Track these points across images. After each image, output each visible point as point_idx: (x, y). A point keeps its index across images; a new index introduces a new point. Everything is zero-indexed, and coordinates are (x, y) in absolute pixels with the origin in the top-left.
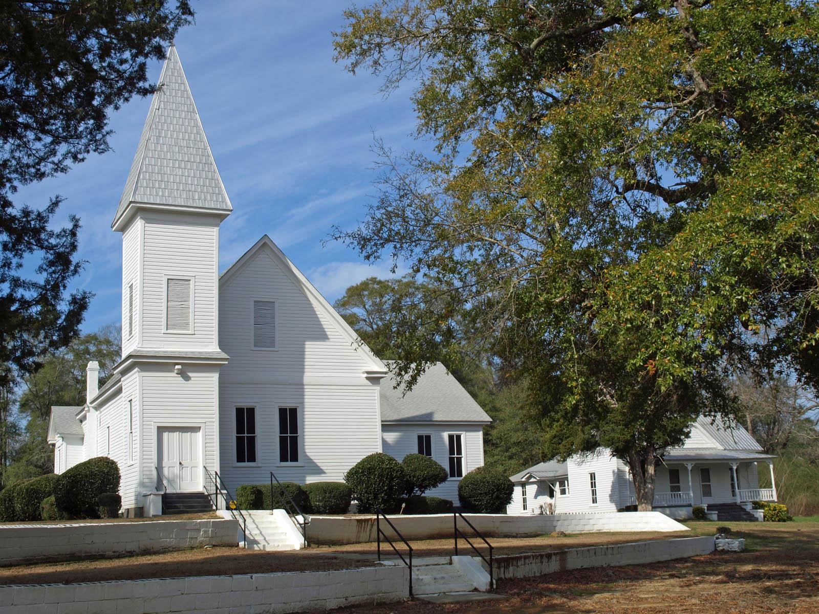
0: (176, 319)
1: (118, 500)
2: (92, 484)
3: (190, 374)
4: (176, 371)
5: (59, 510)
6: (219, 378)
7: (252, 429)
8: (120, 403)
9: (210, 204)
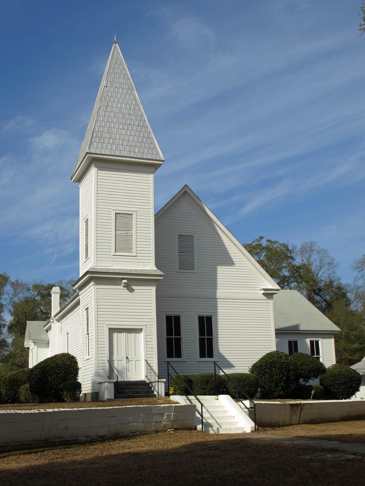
0: (123, 244)
1: (79, 386)
2: (57, 373)
3: (134, 287)
4: (122, 285)
5: (32, 394)
6: (156, 290)
7: (178, 332)
8: (79, 313)
9: (146, 155)
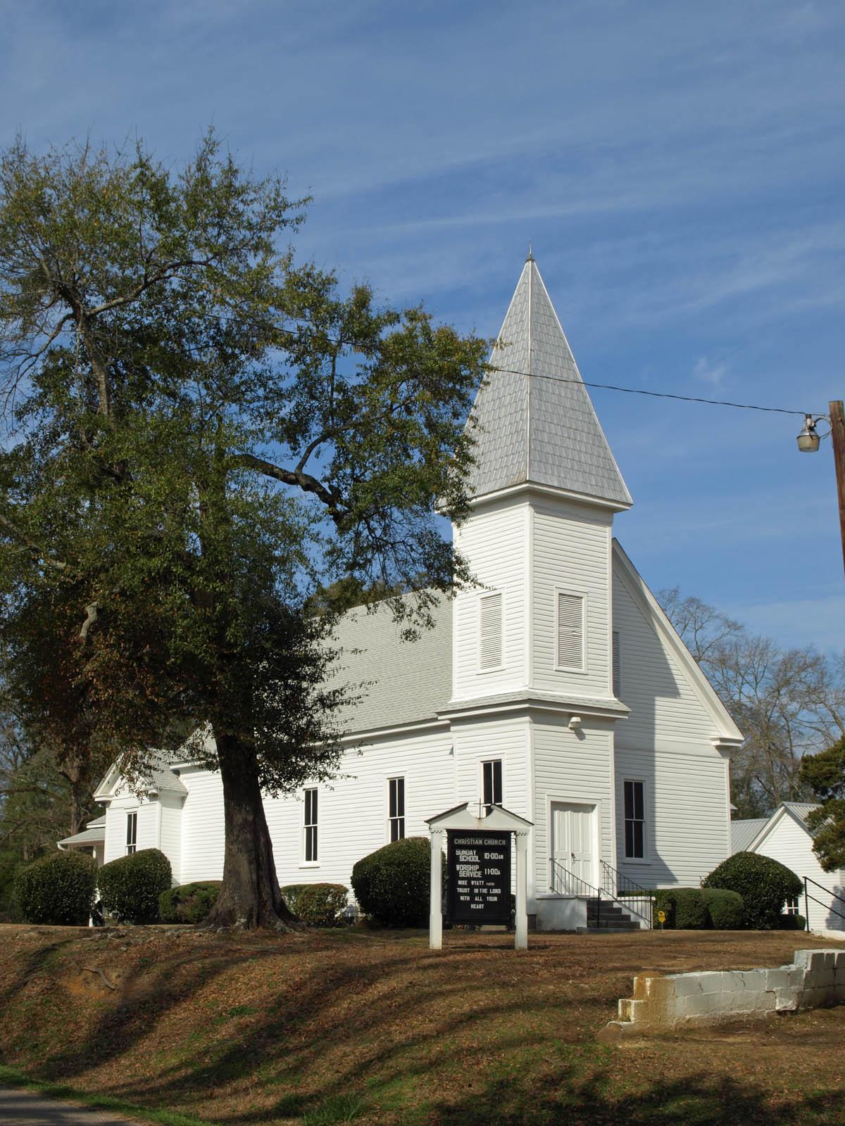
0: (569, 654)
3: (585, 731)
